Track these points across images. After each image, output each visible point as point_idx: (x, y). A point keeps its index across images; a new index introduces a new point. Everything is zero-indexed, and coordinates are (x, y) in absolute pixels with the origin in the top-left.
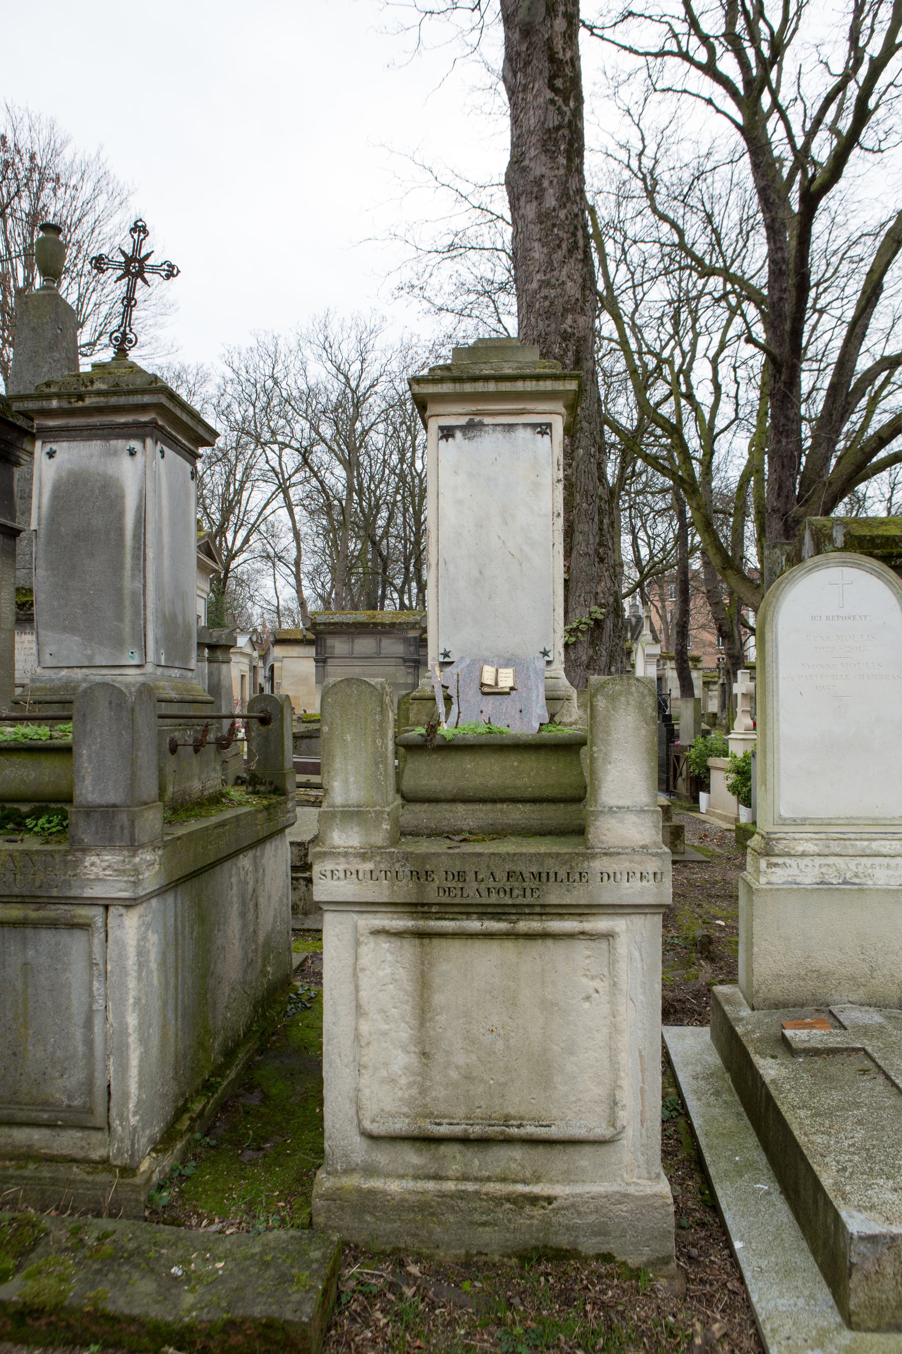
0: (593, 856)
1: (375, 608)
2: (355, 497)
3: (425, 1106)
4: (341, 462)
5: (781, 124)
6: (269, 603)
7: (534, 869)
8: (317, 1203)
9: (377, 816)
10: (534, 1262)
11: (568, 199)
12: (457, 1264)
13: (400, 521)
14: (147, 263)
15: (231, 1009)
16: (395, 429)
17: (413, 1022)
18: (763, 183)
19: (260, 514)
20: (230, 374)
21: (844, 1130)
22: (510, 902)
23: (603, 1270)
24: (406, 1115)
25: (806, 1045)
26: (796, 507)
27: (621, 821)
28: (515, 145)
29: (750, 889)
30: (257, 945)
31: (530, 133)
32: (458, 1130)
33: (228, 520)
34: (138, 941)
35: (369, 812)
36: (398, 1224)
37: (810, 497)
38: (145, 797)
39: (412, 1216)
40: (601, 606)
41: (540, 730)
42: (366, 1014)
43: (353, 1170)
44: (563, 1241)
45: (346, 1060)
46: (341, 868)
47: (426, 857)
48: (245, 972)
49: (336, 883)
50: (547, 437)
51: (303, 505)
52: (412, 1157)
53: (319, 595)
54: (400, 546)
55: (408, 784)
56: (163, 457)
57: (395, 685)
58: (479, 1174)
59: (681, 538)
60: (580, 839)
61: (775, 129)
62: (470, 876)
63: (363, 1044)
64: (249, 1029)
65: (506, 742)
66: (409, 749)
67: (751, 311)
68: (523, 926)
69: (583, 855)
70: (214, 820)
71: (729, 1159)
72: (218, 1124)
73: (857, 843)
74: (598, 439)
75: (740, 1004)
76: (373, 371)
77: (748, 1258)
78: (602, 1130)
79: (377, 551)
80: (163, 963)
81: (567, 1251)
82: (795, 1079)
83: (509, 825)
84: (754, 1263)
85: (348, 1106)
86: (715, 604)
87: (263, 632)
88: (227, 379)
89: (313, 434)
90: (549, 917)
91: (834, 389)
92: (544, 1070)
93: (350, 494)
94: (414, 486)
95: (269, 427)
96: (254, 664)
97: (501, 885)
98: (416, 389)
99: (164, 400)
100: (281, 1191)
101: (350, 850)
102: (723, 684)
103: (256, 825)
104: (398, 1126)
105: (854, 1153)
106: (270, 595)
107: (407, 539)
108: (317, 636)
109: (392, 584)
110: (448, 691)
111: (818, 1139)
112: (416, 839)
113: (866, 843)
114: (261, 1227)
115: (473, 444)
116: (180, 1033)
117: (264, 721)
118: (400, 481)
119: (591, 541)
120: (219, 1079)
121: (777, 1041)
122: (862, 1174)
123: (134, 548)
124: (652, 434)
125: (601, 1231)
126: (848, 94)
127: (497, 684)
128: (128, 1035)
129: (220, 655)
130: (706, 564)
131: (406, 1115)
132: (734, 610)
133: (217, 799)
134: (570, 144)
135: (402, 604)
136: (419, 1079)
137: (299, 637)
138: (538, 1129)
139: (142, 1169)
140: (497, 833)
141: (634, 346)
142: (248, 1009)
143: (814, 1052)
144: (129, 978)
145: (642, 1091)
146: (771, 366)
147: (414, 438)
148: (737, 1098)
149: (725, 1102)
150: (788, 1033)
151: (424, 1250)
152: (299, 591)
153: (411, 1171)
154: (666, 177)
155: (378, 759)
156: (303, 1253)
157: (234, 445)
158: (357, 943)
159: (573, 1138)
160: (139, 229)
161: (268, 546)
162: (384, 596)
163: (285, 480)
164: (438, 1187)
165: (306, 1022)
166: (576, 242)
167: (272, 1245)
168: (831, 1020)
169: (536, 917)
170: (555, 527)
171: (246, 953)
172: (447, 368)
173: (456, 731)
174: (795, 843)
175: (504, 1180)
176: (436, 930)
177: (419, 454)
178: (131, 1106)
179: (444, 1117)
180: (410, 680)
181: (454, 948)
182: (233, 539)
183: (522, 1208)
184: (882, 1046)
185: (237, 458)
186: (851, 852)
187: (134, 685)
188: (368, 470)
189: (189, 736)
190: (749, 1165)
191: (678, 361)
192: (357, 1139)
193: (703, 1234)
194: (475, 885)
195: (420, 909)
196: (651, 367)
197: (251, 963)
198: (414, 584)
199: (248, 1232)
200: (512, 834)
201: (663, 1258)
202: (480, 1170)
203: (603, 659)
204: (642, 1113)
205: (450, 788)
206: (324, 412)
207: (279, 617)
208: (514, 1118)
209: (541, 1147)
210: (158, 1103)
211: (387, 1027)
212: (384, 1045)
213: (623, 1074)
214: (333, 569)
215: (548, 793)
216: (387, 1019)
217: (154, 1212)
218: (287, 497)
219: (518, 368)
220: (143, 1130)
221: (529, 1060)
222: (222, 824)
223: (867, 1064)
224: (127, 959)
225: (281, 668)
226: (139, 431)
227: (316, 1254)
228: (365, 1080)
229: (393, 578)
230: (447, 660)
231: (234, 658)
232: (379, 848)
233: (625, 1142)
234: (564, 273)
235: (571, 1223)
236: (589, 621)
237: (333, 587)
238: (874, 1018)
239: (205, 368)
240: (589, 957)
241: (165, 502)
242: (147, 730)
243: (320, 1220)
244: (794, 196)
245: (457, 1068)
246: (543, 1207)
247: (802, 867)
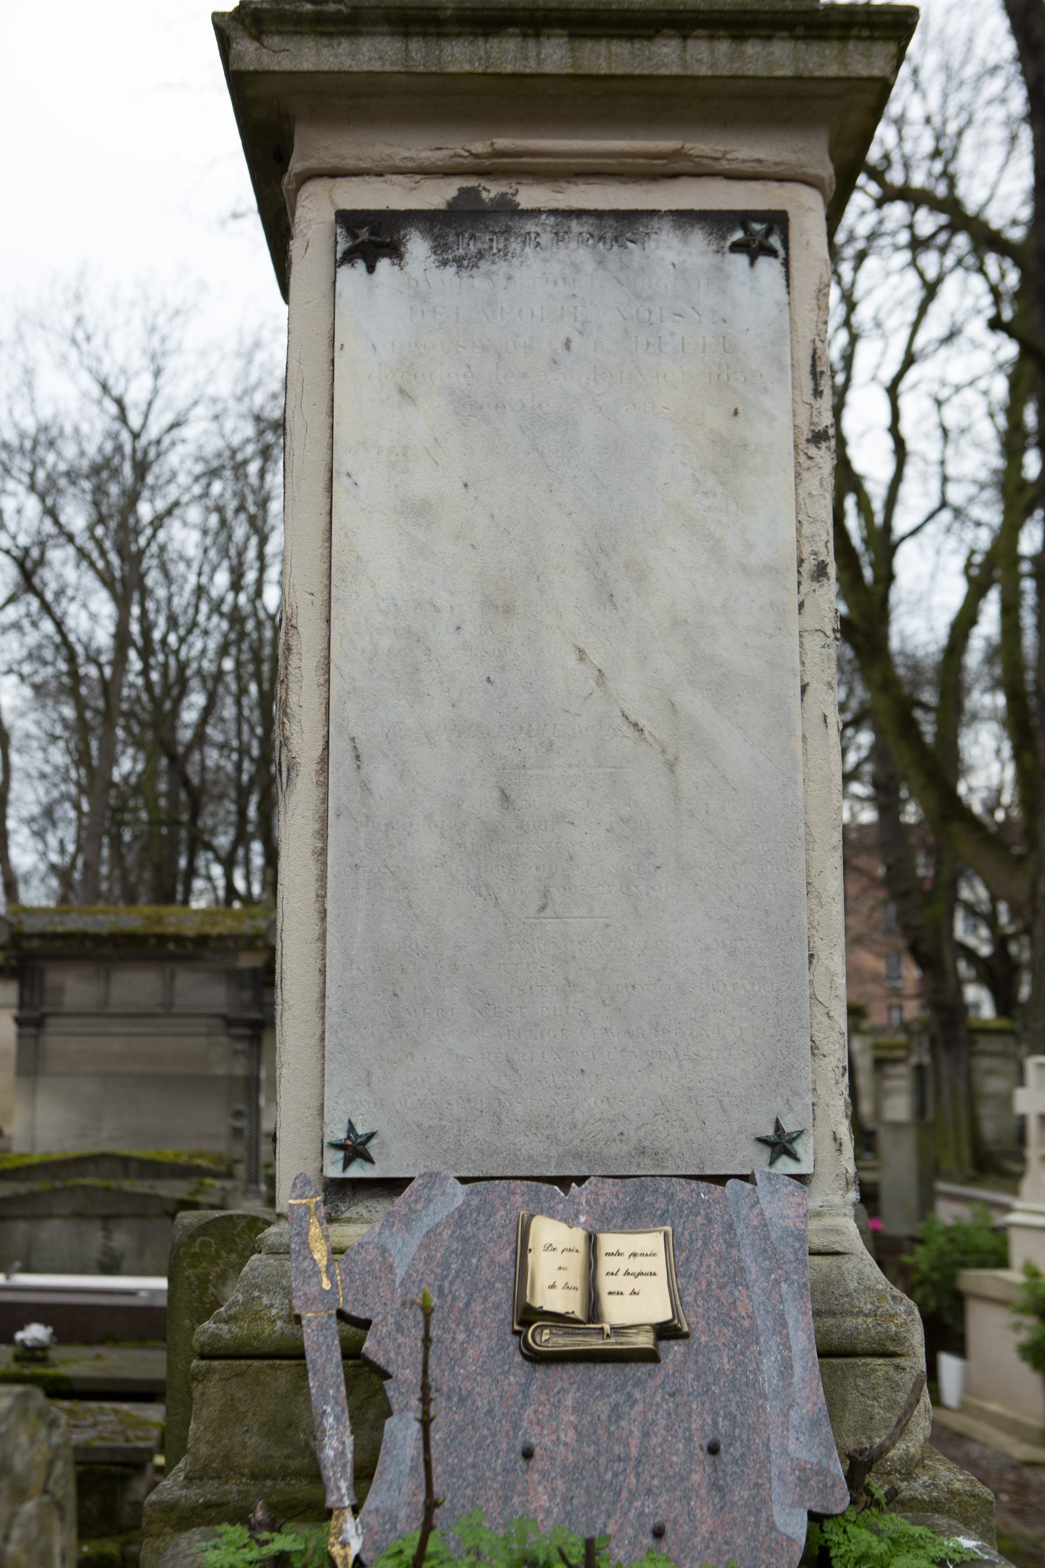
2: (133, 654)
13: (229, 711)
50: (768, 268)
76: (177, 391)
94: (260, 639)
102: (919, 1069)
107: (243, 751)
109: (209, 847)
115: (477, 283)
135: (230, 888)
147: (263, 541)
162: (191, 872)
170: (810, 620)
177: (273, 573)
180: (240, 1068)
198: (257, 847)
229: (213, 832)
230: (358, 1171)
237: (79, 849)
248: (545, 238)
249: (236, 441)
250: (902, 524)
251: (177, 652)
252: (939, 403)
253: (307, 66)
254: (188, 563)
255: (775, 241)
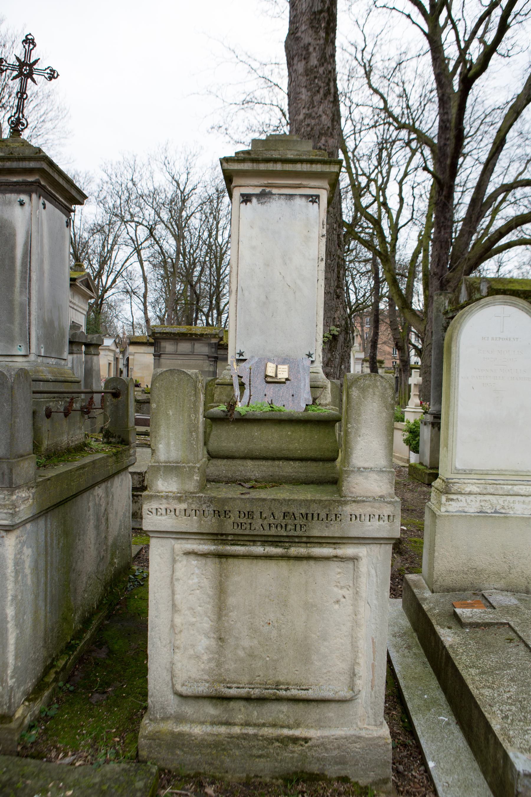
0: (346, 503)
1: (191, 325)
2: (181, 257)
3: (220, 675)
4: (173, 235)
5: (453, 32)
6: (127, 320)
7: (303, 511)
8: (142, 741)
9: (190, 470)
10: (294, 783)
11: (326, 60)
12: (240, 784)
13: (208, 273)
14: (35, 67)
15: (87, 588)
16: (206, 217)
17: (212, 617)
18: (438, 71)
19: (123, 266)
20: (106, 178)
21: (503, 685)
22: (285, 534)
23: (342, 789)
24: (207, 681)
25: (471, 620)
26: (448, 273)
27: (366, 478)
28: (291, 22)
29: (434, 515)
30: (107, 546)
31: (302, 14)
32: (243, 692)
33: (103, 268)
34: (15, 555)
35: (184, 467)
36: (199, 756)
37: (457, 267)
38: (21, 452)
39: (209, 751)
40: (337, 326)
41: (306, 410)
42: (179, 611)
43: (168, 718)
44: (315, 768)
45: (164, 642)
46: (163, 507)
47: (225, 501)
48: (98, 565)
49: (159, 518)
50: (316, 205)
51: (149, 261)
52: (211, 710)
53: (158, 316)
54: (207, 289)
55: (214, 444)
56: (44, 208)
57: (203, 372)
58: (257, 722)
59: (376, 288)
60: (334, 488)
61: (448, 38)
62: (257, 515)
63: (176, 632)
64: (101, 602)
65: (283, 417)
66: (214, 420)
67: (427, 152)
68: (294, 551)
69: (339, 502)
70: (77, 464)
71: (421, 697)
72: (76, 673)
73: (505, 486)
74: (338, 219)
75: (424, 588)
76: (194, 180)
77: (438, 775)
78: (344, 693)
79: (193, 293)
80: (35, 568)
81: (317, 775)
82: (465, 644)
83: (283, 476)
84: (443, 779)
85: (165, 674)
86: (394, 330)
87: (124, 338)
88: (104, 181)
89: (157, 217)
90: (312, 545)
91: (474, 201)
92: (305, 651)
93: (178, 255)
95: (130, 212)
96: (117, 356)
97: (279, 522)
98: (226, 166)
99: (45, 166)
100: (117, 728)
101: (170, 494)
102: (396, 377)
103: (108, 466)
104: (200, 689)
105: (511, 704)
106: (128, 315)
107: (211, 284)
108: (155, 340)
109: (202, 311)
110: (242, 380)
111: (487, 692)
112: (218, 485)
113: (510, 487)
114: (101, 760)
115: (265, 207)
116: (48, 615)
117: (116, 395)
118: (208, 248)
119: (332, 285)
120: (77, 642)
121: (450, 615)
122: (519, 721)
123: (22, 272)
124: (361, 226)
125: (341, 761)
126: (492, 18)
127: (276, 376)
128: (7, 622)
129: (92, 350)
130: (391, 305)
131: (207, 681)
132: (405, 334)
133: (81, 448)
134: (328, 23)
135: (208, 323)
136: (217, 656)
137: (145, 341)
138: (300, 692)
139: (17, 715)
140: (276, 482)
141: (354, 171)
142: (100, 589)
143: (476, 625)
144: (8, 582)
145: (373, 666)
146: (437, 186)
147: (218, 223)
148: (422, 651)
149: (415, 654)
150: (458, 611)
151: (217, 774)
152: (145, 313)
153: (209, 719)
154: (380, 65)
155: (192, 429)
156: (130, 783)
157: (108, 222)
158: (174, 561)
159: (323, 698)
160: (29, 41)
161: (127, 285)
162: (197, 318)
163: (138, 246)
164: (228, 731)
165: (140, 595)
166: (329, 90)
167: (109, 776)
168: (484, 601)
169: (303, 545)
170: (320, 268)
171: (99, 553)
172: (248, 152)
173: (248, 409)
174: (465, 486)
175: (274, 726)
176: (231, 553)
177: (220, 232)
178: (9, 672)
179: (234, 683)
180: (211, 369)
181: (244, 565)
182: (106, 280)
183: (287, 746)
184: (520, 622)
185: (109, 231)
186: (501, 492)
187: (14, 370)
188: (189, 241)
189: (61, 406)
190: (434, 702)
191: (380, 182)
192: (172, 697)
193: (405, 753)
194: (260, 521)
195: (220, 537)
196: (363, 185)
197: (103, 559)
198: (215, 311)
199: (92, 764)
200: (285, 483)
201: (384, 780)
202: (258, 719)
203: (337, 360)
204: (372, 681)
205: (242, 449)
206: (163, 204)
207: (133, 328)
208: (283, 684)
209: (301, 704)
210: (30, 666)
211: (194, 620)
212: (192, 632)
213: (360, 655)
214: (166, 301)
215: (312, 454)
216: (194, 614)
217: (24, 748)
218: (139, 255)
219: (297, 155)
220: (18, 687)
221: (295, 644)
222: (83, 467)
223: (512, 634)
224: (7, 568)
225: (133, 359)
226: (27, 188)
227: (140, 784)
228: (178, 657)
229: (203, 307)
230: (241, 358)
231: (102, 353)
232: (191, 493)
233: (360, 701)
234: (321, 109)
235: (321, 756)
236: (329, 336)
237: (166, 311)
238: (511, 600)
239: (90, 173)
240: (340, 573)
241: (46, 241)
242: (24, 404)
243: (144, 753)
244: (456, 80)
245: (244, 649)
246: (302, 745)
247: (469, 501)
248: (277, 199)
249: (210, 193)
250: (401, 222)
251: (193, 255)
252: (413, 188)
253: (236, 168)
254: (196, 229)
255: (317, 200)
